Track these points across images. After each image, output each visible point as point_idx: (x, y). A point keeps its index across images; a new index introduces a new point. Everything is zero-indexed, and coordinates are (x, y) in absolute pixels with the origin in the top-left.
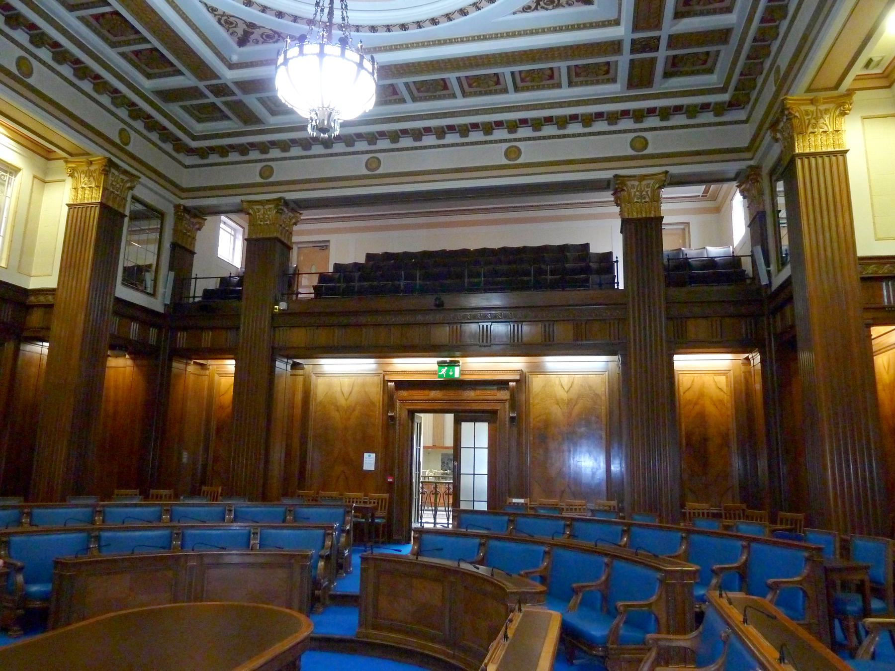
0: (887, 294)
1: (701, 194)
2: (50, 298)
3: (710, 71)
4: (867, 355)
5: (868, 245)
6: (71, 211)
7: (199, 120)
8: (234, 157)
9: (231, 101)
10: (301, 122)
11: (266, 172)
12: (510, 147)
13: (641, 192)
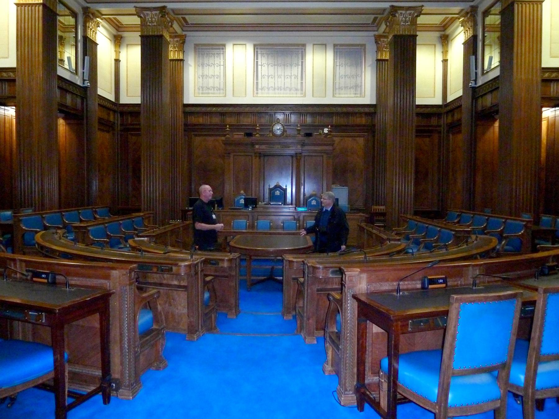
0: (554, 89)
1: (370, 22)
2: (11, 74)
4: (541, 113)
5: (548, 62)
6: (19, 8)
13: (406, 18)
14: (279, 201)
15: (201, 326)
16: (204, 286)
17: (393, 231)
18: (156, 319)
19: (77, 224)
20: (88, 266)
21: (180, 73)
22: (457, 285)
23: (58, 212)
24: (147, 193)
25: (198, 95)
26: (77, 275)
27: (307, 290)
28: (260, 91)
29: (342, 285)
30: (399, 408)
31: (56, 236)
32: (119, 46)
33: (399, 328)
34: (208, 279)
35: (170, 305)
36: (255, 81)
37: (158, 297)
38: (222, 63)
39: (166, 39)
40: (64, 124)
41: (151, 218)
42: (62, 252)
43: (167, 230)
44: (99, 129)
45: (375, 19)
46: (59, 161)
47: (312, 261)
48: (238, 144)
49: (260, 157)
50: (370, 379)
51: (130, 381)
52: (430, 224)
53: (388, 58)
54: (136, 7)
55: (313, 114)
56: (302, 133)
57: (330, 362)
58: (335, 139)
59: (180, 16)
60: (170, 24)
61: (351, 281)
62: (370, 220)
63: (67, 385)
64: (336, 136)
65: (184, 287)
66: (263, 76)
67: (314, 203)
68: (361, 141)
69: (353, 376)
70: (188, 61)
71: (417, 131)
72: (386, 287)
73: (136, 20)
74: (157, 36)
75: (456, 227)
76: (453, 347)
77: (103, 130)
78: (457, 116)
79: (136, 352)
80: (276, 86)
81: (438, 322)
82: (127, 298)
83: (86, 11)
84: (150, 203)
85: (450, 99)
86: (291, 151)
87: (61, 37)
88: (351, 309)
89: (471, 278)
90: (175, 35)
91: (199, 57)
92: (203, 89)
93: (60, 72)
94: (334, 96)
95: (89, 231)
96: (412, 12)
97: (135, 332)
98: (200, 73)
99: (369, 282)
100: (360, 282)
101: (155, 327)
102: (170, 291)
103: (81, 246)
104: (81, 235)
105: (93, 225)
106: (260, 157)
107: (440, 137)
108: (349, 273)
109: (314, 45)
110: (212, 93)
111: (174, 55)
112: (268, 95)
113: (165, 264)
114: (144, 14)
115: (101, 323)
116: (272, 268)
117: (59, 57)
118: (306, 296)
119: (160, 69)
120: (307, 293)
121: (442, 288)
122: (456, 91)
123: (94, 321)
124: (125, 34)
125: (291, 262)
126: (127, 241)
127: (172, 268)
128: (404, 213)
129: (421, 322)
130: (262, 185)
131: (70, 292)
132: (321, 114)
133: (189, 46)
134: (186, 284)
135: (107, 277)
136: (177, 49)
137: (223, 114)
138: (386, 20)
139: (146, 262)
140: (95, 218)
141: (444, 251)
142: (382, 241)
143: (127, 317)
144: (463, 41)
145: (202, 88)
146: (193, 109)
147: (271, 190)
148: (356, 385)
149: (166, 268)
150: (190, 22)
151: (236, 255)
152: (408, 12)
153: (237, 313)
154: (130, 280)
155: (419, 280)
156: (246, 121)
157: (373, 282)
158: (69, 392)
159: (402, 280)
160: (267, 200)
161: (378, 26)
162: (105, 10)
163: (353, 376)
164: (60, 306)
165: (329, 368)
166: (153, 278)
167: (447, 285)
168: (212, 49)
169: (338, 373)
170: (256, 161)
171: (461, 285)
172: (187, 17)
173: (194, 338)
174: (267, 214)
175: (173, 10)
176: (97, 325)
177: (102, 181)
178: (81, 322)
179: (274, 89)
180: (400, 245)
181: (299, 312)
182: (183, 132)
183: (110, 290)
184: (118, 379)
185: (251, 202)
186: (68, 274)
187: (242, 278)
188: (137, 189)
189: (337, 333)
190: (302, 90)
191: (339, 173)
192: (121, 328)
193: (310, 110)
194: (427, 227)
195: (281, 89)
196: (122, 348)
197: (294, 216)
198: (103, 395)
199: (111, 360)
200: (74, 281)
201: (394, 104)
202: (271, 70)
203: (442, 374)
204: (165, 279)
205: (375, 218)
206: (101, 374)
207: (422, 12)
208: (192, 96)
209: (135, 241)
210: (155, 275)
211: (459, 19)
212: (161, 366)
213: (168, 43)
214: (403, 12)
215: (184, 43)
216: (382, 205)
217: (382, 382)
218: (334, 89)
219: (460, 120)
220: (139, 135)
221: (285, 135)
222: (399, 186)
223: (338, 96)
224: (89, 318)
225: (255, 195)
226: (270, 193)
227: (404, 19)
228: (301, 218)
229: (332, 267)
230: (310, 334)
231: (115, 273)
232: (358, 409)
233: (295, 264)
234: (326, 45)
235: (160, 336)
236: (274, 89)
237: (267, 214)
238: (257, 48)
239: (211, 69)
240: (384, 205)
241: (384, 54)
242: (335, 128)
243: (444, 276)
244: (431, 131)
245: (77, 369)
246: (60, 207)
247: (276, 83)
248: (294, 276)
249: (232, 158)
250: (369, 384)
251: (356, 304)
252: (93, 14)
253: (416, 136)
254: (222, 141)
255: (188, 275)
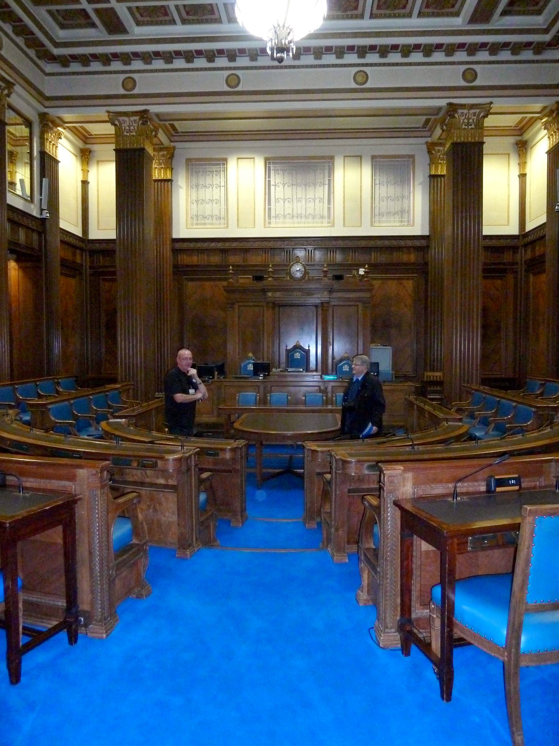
1: (421, 125)
3: (457, 14)
7: (63, 27)
8: (201, 62)
9: (102, 9)
10: (239, 32)
11: (129, 84)
12: (468, 69)
13: (469, 119)
14: (300, 368)
15: (196, 539)
16: (199, 486)
17: (453, 406)
18: (136, 531)
19: (36, 401)
20: (48, 463)
21: (168, 197)
22: (535, 487)
23: (11, 385)
24: (125, 358)
25: (191, 227)
26: (35, 475)
27: (336, 491)
28: (273, 220)
29: (381, 488)
30: (456, 651)
31: (7, 419)
32: (88, 163)
33: (456, 546)
34: (205, 475)
35: (155, 510)
36: (267, 207)
37: (139, 502)
38: (223, 184)
39: (149, 154)
40: (17, 267)
41: (131, 391)
42: (15, 441)
43: (151, 407)
44: (62, 274)
45: (427, 121)
46: (10, 315)
47: (342, 451)
48: (244, 291)
49: (273, 308)
50: (418, 612)
51: (103, 614)
52: (502, 398)
53: (444, 172)
54: (108, 112)
55: (344, 250)
56: (330, 275)
57: (366, 589)
58: (374, 282)
59: (167, 123)
60: (154, 133)
61: (391, 482)
62: (422, 392)
63: (21, 620)
64: (375, 279)
65: (173, 487)
66: (277, 200)
67: (346, 368)
68: (409, 285)
69: (395, 609)
70: (177, 181)
71: (485, 271)
72: (438, 490)
73: (109, 129)
74: (135, 150)
75: (538, 402)
76: (526, 576)
77: (67, 275)
78: (538, 250)
79: (110, 576)
80: (295, 213)
81: (508, 539)
82: (98, 501)
83: (43, 116)
84: (129, 370)
85: (530, 226)
86: (315, 299)
87: (11, 154)
88: (391, 519)
89: (554, 477)
90: (160, 148)
91: (192, 175)
92: (198, 218)
93: (11, 200)
94: (372, 225)
95: (49, 410)
96: (478, 111)
97: (108, 549)
98: (194, 198)
99: (416, 484)
100: (404, 483)
101: (135, 541)
102: (155, 493)
103: (38, 432)
104: (40, 419)
105: (56, 402)
106: (273, 308)
107: (516, 278)
108: (389, 472)
109: (345, 157)
110: (209, 224)
111: (159, 174)
112: (284, 225)
113: (148, 457)
114: (119, 122)
115: (65, 538)
116: (291, 457)
117: (8, 178)
118: (333, 499)
119: (141, 186)
120: (336, 495)
121: (514, 491)
122: (537, 217)
123: (56, 535)
124: (95, 147)
125: (314, 451)
126: (98, 423)
127: (156, 463)
128: (468, 383)
129: (484, 539)
130: (276, 345)
131: (24, 498)
132: (355, 249)
133: (179, 162)
134: (175, 483)
135: (72, 478)
136: (163, 166)
137: (224, 251)
138: (443, 123)
139: (123, 455)
140: (58, 392)
141: (520, 436)
142: (436, 421)
143: (98, 530)
144: (547, 149)
145: (197, 216)
146: (185, 245)
147: (288, 351)
148: (400, 620)
149: (148, 463)
150: (180, 130)
151: (241, 443)
152: (472, 111)
153: (244, 519)
154: (101, 482)
155: (483, 480)
156: (256, 259)
157: (422, 484)
158: (24, 628)
159: (460, 480)
160: (283, 365)
161: (432, 131)
162: (68, 116)
163: (395, 609)
164: (12, 517)
165: (364, 596)
166: (133, 475)
167: (520, 488)
168: (210, 164)
169: (376, 604)
170: (268, 314)
171: (540, 487)
172: (176, 123)
173: (187, 555)
174: (282, 385)
175: (157, 115)
176: (60, 541)
177: (66, 341)
178: (38, 537)
179: (293, 217)
180: (460, 427)
181: (325, 519)
182: (172, 275)
183: (76, 495)
184: (88, 612)
185: (262, 368)
186: (22, 473)
187: (249, 470)
188: (112, 352)
189: (374, 550)
190: (329, 217)
191: (380, 328)
192: (90, 544)
193: (341, 244)
194: (499, 401)
195: (301, 217)
196: (91, 570)
197: (319, 387)
198: (68, 631)
199: (78, 585)
200: (30, 482)
201: (454, 237)
202: (288, 191)
203: (512, 613)
204: (148, 477)
205: (429, 389)
206: (65, 605)
207: (491, 111)
208: (184, 228)
209: (109, 424)
210: (135, 472)
211: (541, 119)
212: (144, 592)
213: (151, 159)
214: (465, 111)
215: (172, 157)
216: (437, 371)
217: (433, 618)
218: (373, 215)
219: (543, 256)
220: (114, 280)
221: (307, 278)
222: (462, 344)
223: (377, 225)
224: (50, 532)
225: (268, 358)
226: (287, 355)
227: (466, 121)
228: (329, 389)
229: (368, 461)
230: (340, 549)
231: (82, 473)
232: (403, 653)
233: (320, 454)
234: (361, 157)
235: (142, 554)
236: (293, 217)
237: (282, 385)
238: (269, 163)
239: (208, 191)
240: (440, 371)
241: (439, 168)
242: (374, 267)
243: (517, 476)
244: (504, 271)
245: (34, 598)
246: (12, 379)
247: (295, 207)
248: (318, 471)
249: (237, 310)
250: (418, 619)
251: (398, 513)
252: (53, 122)
253: (484, 277)
254: (224, 287)
255: (178, 471)
